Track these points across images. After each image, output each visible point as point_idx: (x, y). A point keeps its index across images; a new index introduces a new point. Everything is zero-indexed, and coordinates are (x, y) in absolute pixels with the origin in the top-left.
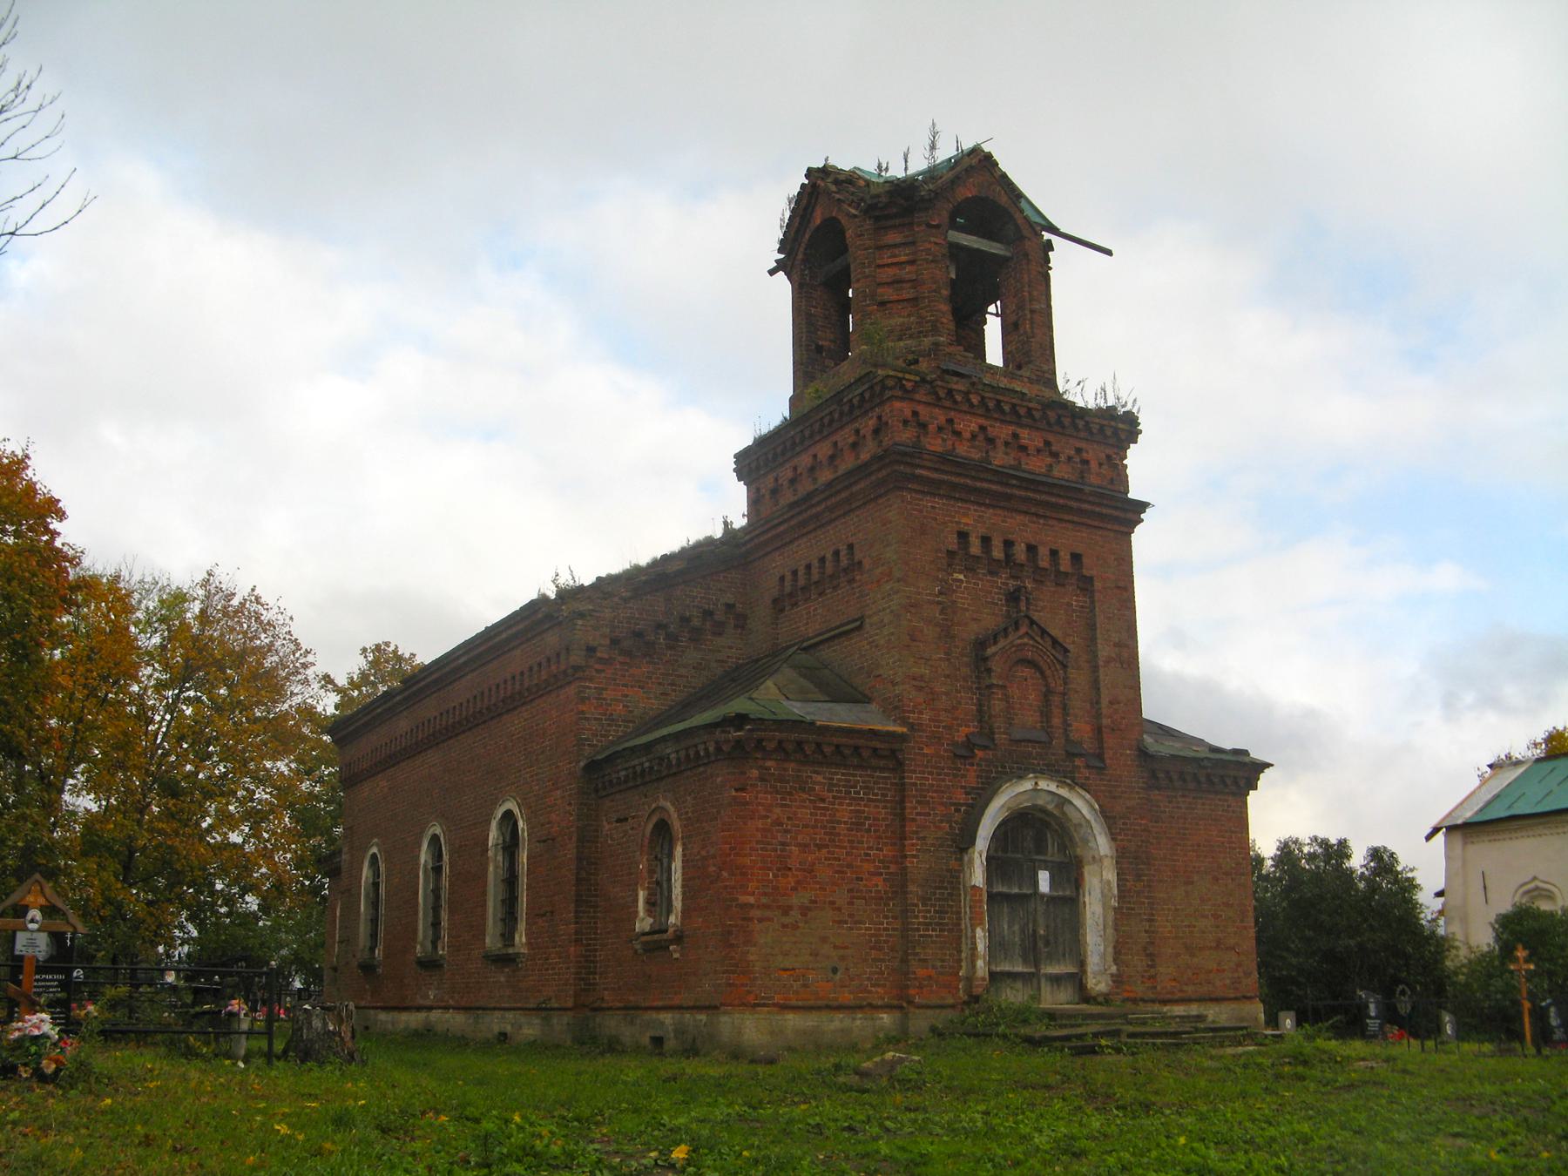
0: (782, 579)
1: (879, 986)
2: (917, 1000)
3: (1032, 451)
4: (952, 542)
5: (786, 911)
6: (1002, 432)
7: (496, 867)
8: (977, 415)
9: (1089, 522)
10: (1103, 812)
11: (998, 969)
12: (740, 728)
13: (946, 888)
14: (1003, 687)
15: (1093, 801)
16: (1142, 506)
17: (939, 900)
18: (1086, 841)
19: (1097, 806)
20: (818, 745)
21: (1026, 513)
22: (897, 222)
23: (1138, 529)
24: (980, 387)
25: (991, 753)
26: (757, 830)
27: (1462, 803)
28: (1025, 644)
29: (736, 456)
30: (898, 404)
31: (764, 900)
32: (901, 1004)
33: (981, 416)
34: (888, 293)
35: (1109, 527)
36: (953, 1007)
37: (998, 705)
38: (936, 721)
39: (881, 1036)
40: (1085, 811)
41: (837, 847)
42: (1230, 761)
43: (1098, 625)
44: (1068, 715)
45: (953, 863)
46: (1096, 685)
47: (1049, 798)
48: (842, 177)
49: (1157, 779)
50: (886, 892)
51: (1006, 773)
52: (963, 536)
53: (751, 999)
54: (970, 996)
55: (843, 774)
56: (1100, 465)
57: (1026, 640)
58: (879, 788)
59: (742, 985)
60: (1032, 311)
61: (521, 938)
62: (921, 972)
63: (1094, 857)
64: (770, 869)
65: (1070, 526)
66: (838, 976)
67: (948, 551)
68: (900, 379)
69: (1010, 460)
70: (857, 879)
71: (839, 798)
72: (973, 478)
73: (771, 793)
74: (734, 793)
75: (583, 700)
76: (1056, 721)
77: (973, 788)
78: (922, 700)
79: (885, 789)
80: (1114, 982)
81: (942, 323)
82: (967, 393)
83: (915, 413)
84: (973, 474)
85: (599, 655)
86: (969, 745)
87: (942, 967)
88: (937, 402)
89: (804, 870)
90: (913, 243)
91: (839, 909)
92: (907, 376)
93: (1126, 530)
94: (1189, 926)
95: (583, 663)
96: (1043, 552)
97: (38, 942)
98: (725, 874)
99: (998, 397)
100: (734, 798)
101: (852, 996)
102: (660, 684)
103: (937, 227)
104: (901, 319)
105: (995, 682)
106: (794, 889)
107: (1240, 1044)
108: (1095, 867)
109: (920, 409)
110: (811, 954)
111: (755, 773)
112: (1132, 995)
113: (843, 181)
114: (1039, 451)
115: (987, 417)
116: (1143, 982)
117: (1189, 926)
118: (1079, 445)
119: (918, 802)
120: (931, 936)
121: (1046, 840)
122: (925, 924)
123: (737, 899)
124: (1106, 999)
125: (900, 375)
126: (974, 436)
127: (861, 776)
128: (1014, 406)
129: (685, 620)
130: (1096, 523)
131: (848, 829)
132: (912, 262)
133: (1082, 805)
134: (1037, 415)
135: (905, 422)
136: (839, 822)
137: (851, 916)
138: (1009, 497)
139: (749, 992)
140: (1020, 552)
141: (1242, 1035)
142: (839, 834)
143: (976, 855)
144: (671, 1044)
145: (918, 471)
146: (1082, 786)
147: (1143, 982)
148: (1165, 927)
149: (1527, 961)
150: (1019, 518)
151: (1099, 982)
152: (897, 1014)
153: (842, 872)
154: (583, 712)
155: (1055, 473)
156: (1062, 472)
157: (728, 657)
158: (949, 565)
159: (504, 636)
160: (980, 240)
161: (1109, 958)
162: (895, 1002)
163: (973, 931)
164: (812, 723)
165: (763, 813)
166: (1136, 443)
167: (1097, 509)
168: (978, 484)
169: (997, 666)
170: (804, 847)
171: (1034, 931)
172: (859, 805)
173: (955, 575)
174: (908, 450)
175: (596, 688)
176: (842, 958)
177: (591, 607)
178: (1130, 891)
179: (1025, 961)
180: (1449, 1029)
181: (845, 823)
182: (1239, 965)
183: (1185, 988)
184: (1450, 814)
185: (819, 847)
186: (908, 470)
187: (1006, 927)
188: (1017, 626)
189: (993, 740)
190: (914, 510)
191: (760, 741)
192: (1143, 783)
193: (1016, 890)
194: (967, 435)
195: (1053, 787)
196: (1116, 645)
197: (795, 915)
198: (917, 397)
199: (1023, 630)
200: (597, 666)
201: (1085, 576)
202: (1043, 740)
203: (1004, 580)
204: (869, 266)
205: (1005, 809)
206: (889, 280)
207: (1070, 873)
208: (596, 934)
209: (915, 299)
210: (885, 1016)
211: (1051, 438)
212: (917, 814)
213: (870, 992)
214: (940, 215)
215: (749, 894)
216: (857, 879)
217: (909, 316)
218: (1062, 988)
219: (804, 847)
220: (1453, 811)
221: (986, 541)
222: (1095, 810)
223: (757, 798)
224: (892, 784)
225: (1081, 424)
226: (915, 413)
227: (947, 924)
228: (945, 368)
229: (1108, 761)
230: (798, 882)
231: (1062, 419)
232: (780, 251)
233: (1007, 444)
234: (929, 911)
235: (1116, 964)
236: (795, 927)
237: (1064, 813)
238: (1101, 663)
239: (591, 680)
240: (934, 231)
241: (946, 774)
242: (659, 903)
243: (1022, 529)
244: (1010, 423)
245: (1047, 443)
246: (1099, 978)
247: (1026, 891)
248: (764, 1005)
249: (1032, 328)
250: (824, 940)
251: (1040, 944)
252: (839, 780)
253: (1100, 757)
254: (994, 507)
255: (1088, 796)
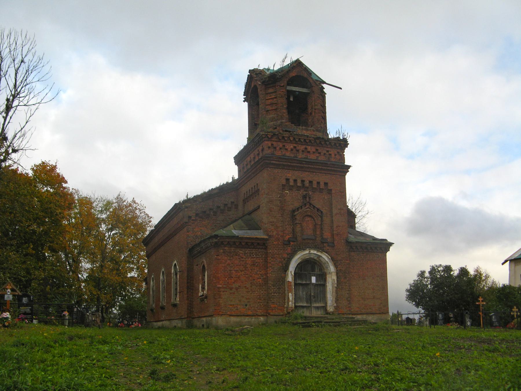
0: (245, 194)
1: (260, 310)
2: (271, 313)
3: (311, 152)
4: (284, 182)
5: (231, 289)
6: (302, 148)
7: (174, 280)
8: (293, 143)
9: (330, 173)
10: (332, 259)
11: (298, 305)
12: (217, 239)
13: (280, 282)
14: (300, 223)
15: (328, 256)
16: (349, 167)
17: (278, 285)
18: (327, 268)
19: (330, 257)
20: (240, 242)
21: (309, 172)
22: (272, 85)
23: (348, 174)
24: (293, 135)
25: (296, 243)
26: (222, 267)
27: (518, 251)
28: (308, 211)
29: (234, 158)
30: (266, 142)
31: (224, 286)
32: (266, 315)
33: (294, 143)
34: (269, 108)
35: (338, 174)
36: (282, 315)
37: (298, 229)
38: (278, 234)
39: (260, 323)
40: (326, 259)
41: (247, 271)
42: (378, 243)
43: (333, 204)
44: (323, 231)
45: (283, 275)
46: (332, 222)
47: (315, 255)
48: (258, 72)
49: (353, 249)
50: (262, 283)
51: (299, 249)
52: (288, 180)
53: (221, 313)
54: (288, 312)
55: (249, 250)
56: (335, 155)
57: (308, 209)
58: (260, 254)
59: (218, 309)
60: (315, 109)
61: (178, 299)
62: (272, 306)
63: (330, 272)
64: (226, 277)
65: (324, 174)
66: (247, 307)
67: (282, 185)
68: (267, 135)
69: (303, 156)
70: (253, 280)
71: (247, 257)
72: (290, 162)
73: (226, 256)
74: (216, 257)
75: (188, 232)
76: (318, 233)
77: (290, 253)
78: (273, 228)
79: (262, 254)
80: (335, 308)
81: (284, 116)
82: (289, 137)
83: (272, 144)
84: (290, 161)
85: (192, 218)
86: (289, 241)
87: (279, 304)
88: (280, 141)
89: (237, 277)
90: (276, 92)
91: (248, 288)
92: (269, 134)
93: (344, 174)
94: (364, 292)
95: (188, 221)
96: (315, 183)
97: (10, 297)
98: (214, 279)
99: (299, 137)
100: (216, 258)
101: (251, 313)
102: (211, 226)
103: (283, 86)
104: (272, 115)
105: (297, 222)
106: (234, 283)
107: (361, 325)
108: (330, 275)
109: (274, 143)
110: (239, 301)
111: (222, 251)
112: (342, 312)
113: (258, 74)
114: (314, 152)
115: (296, 144)
116: (346, 309)
117: (364, 292)
118: (327, 149)
119: (272, 258)
120: (276, 296)
121: (315, 268)
122: (274, 292)
123: (217, 286)
124: (333, 313)
125: (267, 134)
126: (292, 150)
127: (254, 251)
128: (305, 140)
129: (218, 207)
130: (333, 173)
131: (250, 266)
132: (276, 98)
133: (325, 257)
134: (313, 142)
135: (269, 147)
136: (248, 264)
137: (251, 290)
138: (302, 167)
139: (220, 311)
140: (307, 184)
141: (362, 323)
142: (247, 267)
143: (289, 272)
144: (205, 326)
145: (272, 162)
146: (324, 251)
147: (346, 309)
148: (355, 292)
149: (482, 301)
150: (307, 173)
151: (331, 308)
152: (265, 317)
153: (249, 278)
154: (188, 235)
155: (319, 159)
156: (322, 158)
157: (233, 217)
158: (283, 189)
159: (172, 213)
160: (299, 88)
161: (334, 302)
162: (265, 314)
163: (288, 294)
164: (238, 236)
165: (224, 262)
166: (347, 147)
167: (333, 169)
168: (292, 164)
169: (298, 217)
170: (236, 271)
171: (310, 294)
172: (254, 259)
173: (286, 192)
174: (270, 156)
175: (192, 228)
176: (249, 302)
177: (190, 205)
178: (342, 282)
179: (307, 302)
180: (469, 324)
181: (250, 264)
182: (381, 303)
183: (362, 310)
184: (511, 256)
185: (241, 271)
186: (269, 162)
187: (301, 293)
188: (305, 205)
189: (297, 239)
190: (272, 173)
191: (222, 242)
192: (348, 250)
193: (304, 282)
194: (289, 150)
195: (315, 252)
196: (339, 209)
197: (234, 290)
198: (273, 139)
199: (307, 206)
200: (192, 222)
201: (329, 189)
202: (313, 238)
203: (302, 192)
204: (264, 100)
205: (300, 259)
206: (269, 104)
207: (322, 277)
208: (193, 297)
209: (276, 109)
210: (262, 318)
211: (318, 148)
212: (271, 261)
213: (258, 311)
214: (284, 82)
215: (220, 284)
216: (253, 280)
217: (275, 114)
218: (319, 310)
219: (236, 271)
220: (513, 255)
221: (295, 181)
222: (330, 259)
223: (222, 258)
224: (264, 253)
225: (328, 143)
226: (272, 144)
227: (281, 292)
228: (284, 130)
229: (335, 244)
230: (235, 281)
231: (321, 142)
232: (244, 95)
233: (303, 151)
234: (275, 289)
235: (336, 303)
236: (234, 293)
237: (320, 260)
238: (334, 215)
239: (190, 226)
240: (282, 87)
241: (281, 250)
242: (203, 288)
243: (307, 176)
244: (304, 145)
245: (317, 150)
246: (331, 307)
247: (308, 282)
248: (225, 315)
249: (315, 114)
250: (243, 297)
251: (312, 298)
252: (247, 252)
253: (333, 243)
254: (298, 170)
255: (327, 255)
